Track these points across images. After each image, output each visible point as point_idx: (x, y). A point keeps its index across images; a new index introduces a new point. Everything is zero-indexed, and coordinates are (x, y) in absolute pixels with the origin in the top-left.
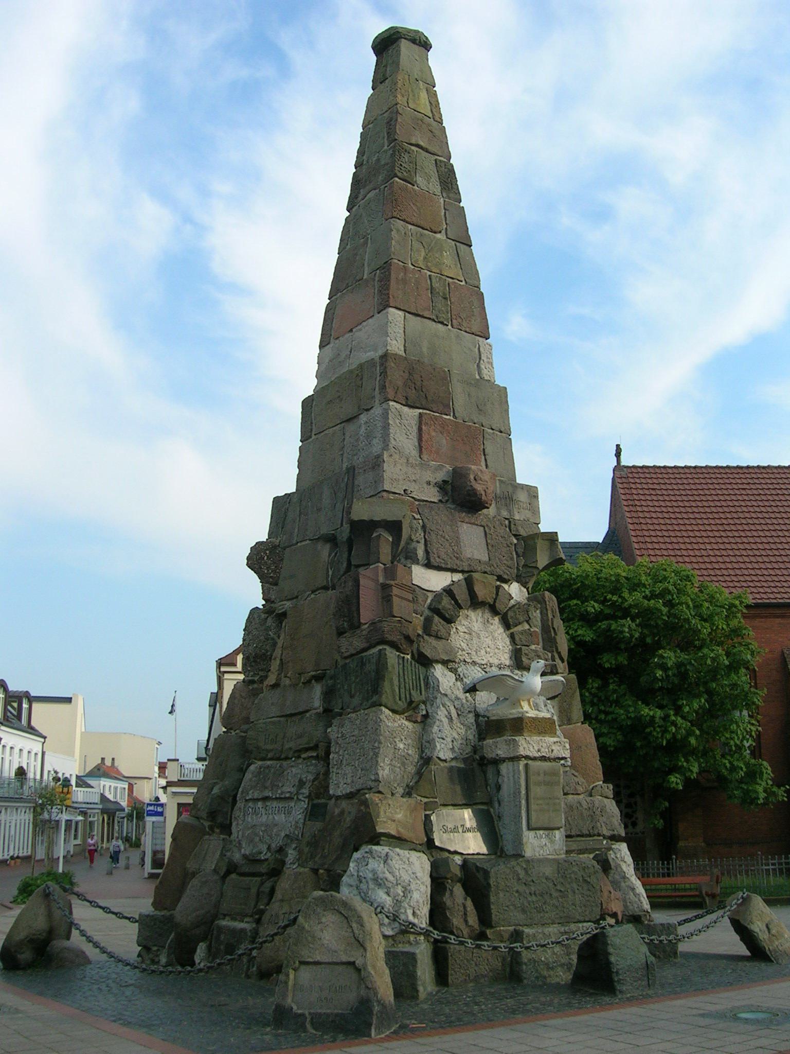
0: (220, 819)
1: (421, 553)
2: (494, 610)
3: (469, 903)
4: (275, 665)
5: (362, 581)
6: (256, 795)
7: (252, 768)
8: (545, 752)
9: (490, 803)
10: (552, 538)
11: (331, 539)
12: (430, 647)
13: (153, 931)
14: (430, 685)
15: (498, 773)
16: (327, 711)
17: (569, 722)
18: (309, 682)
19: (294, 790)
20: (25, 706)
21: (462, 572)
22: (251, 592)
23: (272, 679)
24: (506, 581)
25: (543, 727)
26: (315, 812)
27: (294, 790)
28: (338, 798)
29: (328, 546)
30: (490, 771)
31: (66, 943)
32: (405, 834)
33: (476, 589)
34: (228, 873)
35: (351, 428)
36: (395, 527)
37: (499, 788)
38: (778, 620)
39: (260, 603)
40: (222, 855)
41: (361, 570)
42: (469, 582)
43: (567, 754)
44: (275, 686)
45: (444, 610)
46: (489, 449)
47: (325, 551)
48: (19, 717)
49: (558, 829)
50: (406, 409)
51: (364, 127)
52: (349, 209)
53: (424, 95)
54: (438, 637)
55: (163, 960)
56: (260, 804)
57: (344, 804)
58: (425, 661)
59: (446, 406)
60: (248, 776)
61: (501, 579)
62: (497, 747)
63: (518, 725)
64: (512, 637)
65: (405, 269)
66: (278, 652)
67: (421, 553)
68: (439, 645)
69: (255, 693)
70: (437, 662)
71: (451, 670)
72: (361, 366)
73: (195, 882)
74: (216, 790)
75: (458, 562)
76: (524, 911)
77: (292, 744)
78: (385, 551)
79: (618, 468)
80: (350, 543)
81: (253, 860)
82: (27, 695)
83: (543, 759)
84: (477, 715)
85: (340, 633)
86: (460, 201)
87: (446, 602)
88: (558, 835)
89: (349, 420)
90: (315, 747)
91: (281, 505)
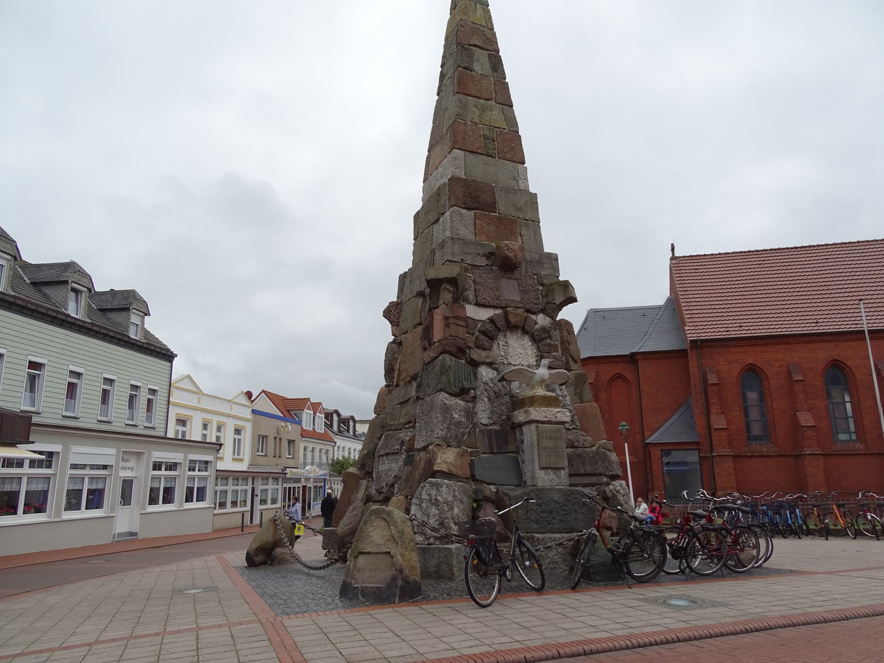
0: (367, 469)
1: (471, 297)
2: (525, 332)
6: (382, 452)
8: (550, 418)
9: (517, 452)
11: (421, 294)
12: (477, 354)
16: (418, 398)
18: (410, 382)
19: (398, 447)
20: (351, 424)
21: (502, 308)
22: (385, 333)
24: (534, 313)
26: (409, 461)
27: (398, 447)
28: (419, 450)
30: (518, 430)
32: (454, 471)
33: (510, 317)
35: (436, 227)
36: (453, 281)
37: (523, 442)
38: (783, 346)
42: (506, 314)
43: (568, 419)
44: (397, 386)
45: (491, 332)
46: (524, 232)
47: (420, 301)
48: (348, 431)
49: (563, 468)
50: (465, 211)
51: (446, 40)
53: (480, 11)
54: (485, 349)
56: (385, 458)
58: (475, 364)
59: (492, 207)
61: (528, 311)
62: (520, 416)
63: (532, 401)
67: (471, 297)
68: (483, 354)
69: (390, 392)
70: (483, 363)
71: (494, 369)
73: (351, 508)
75: (498, 302)
76: (537, 522)
79: (673, 258)
82: (352, 418)
83: (550, 422)
84: (512, 397)
85: (425, 349)
86: (505, 78)
87: (489, 326)
88: (563, 474)
90: (410, 422)
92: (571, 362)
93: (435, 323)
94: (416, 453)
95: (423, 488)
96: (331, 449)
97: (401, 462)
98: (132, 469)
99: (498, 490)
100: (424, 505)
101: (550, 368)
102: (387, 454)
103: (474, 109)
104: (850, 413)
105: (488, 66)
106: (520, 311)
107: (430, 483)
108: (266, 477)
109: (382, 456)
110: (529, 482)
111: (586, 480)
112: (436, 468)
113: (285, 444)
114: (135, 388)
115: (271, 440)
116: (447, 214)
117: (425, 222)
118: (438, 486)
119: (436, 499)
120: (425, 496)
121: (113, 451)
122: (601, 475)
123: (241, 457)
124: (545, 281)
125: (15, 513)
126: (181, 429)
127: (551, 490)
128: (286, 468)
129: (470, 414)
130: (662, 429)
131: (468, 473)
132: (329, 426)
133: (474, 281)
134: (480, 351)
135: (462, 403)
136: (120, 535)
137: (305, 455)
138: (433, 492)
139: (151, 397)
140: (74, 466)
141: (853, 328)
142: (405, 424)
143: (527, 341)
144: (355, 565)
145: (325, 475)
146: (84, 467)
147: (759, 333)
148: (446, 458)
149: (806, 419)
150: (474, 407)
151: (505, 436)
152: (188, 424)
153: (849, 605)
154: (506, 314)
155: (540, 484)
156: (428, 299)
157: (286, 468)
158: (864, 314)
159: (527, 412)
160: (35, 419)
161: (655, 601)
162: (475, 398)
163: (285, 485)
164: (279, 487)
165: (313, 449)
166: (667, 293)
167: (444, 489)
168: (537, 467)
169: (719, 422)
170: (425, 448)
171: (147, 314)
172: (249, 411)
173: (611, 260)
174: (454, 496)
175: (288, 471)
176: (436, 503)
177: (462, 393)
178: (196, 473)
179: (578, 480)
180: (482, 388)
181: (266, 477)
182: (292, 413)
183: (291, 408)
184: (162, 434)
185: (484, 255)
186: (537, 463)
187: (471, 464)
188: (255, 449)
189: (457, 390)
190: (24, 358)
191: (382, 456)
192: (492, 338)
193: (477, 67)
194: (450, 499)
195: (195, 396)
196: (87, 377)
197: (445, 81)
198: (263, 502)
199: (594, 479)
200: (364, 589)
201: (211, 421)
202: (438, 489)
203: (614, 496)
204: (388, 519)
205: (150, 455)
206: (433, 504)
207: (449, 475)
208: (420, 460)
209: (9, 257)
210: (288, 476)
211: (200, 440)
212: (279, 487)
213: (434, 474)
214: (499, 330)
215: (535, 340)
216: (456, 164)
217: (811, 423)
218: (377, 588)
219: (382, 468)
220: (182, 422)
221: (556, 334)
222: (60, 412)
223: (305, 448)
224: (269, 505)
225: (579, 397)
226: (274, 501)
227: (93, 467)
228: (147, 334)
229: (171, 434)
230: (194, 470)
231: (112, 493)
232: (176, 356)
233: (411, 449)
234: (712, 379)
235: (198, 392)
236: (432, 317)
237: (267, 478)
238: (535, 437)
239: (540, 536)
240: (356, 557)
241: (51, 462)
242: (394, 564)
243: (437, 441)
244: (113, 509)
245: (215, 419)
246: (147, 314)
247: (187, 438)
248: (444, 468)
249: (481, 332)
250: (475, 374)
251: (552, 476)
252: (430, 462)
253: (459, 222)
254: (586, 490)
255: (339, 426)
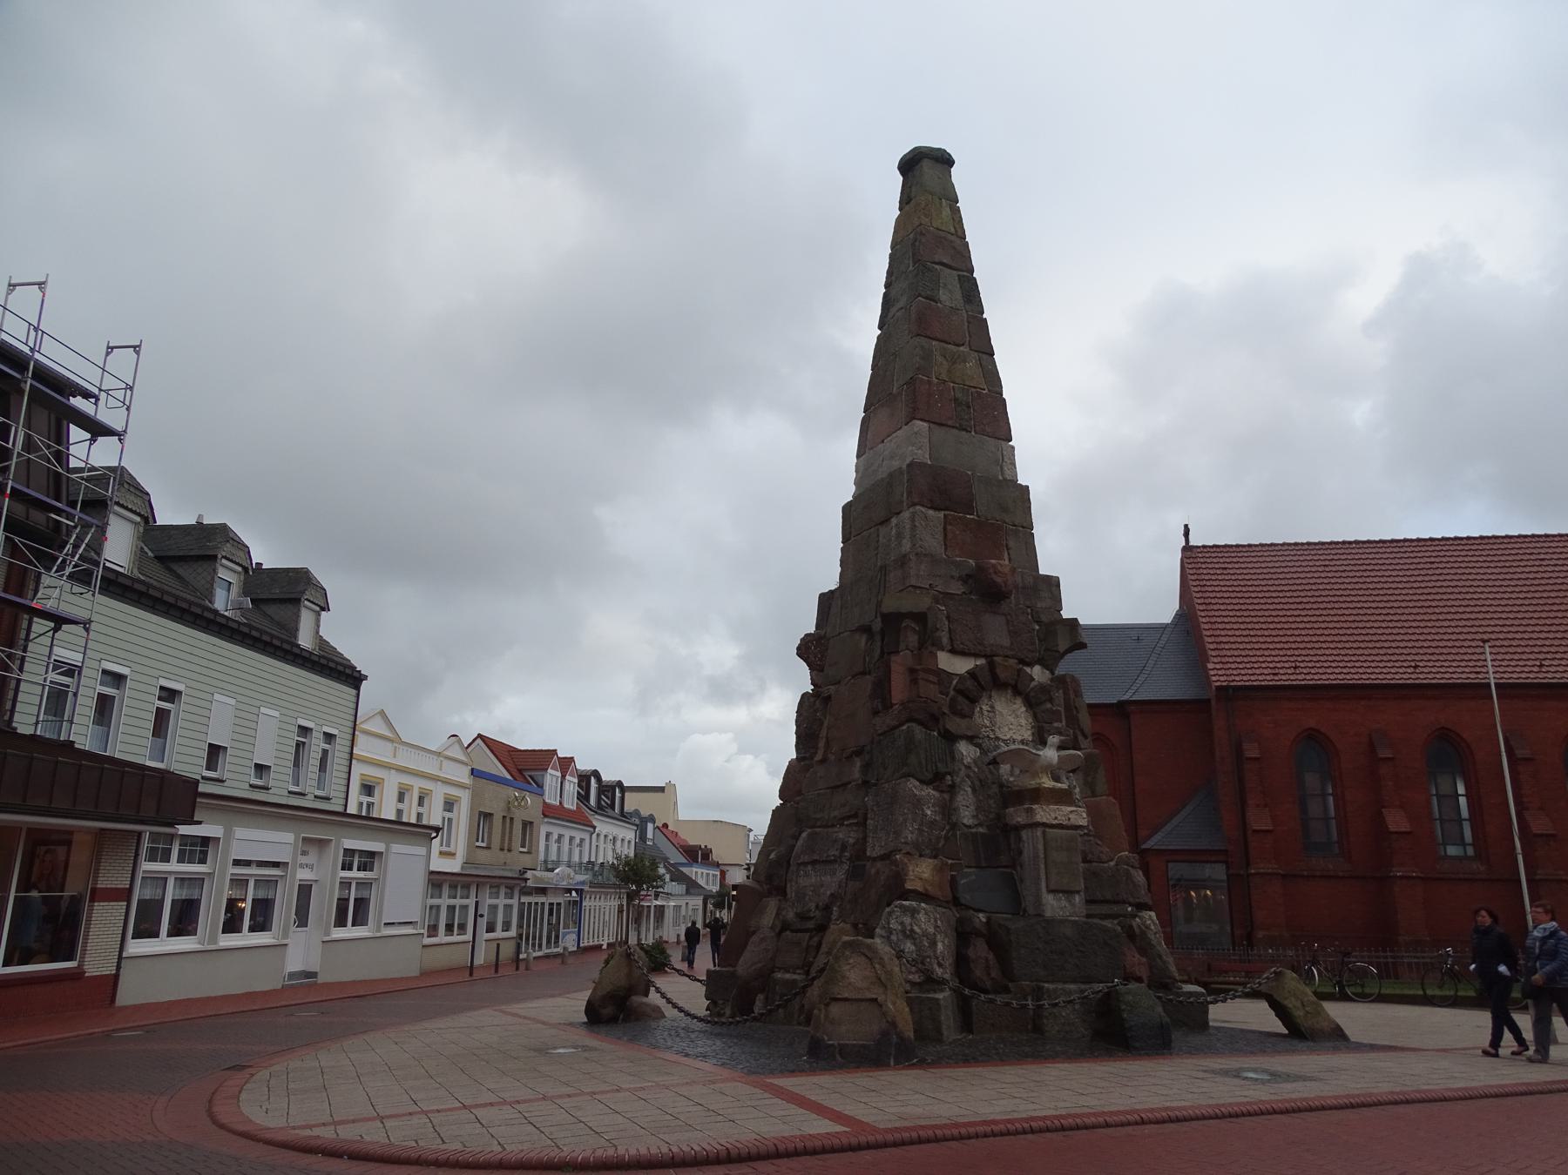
1: (945, 640)
2: (1017, 692)
3: (991, 956)
4: (822, 744)
5: (894, 667)
6: (806, 858)
7: (804, 835)
10: (1074, 622)
11: (866, 630)
12: (954, 724)
13: (715, 985)
14: (953, 755)
15: (1020, 839)
16: (866, 783)
17: (1094, 795)
18: (849, 758)
20: (618, 794)
21: (985, 656)
23: (819, 757)
25: (1063, 797)
26: (856, 873)
28: (874, 859)
29: (864, 638)
31: (645, 1000)
34: (783, 929)
35: (883, 530)
36: (920, 618)
37: (1020, 853)
39: (809, 688)
40: (778, 914)
41: (893, 658)
42: (992, 666)
43: (1084, 823)
44: (823, 761)
46: (1011, 544)
48: (612, 806)
50: (931, 512)
51: (892, 248)
52: (880, 328)
53: (946, 212)
54: (963, 716)
55: (728, 1012)
57: (879, 864)
58: (951, 738)
60: (800, 842)
61: (1022, 662)
62: (1017, 816)
63: (1037, 795)
64: (1035, 716)
65: (929, 383)
66: (824, 733)
67: (945, 640)
68: (963, 723)
72: (891, 475)
73: (754, 938)
74: (772, 856)
77: (836, 813)
78: (913, 639)
79: (1187, 549)
80: (883, 632)
81: (803, 917)
82: (620, 784)
84: (1001, 786)
85: (876, 713)
87: (969, 684)
89: (882, 523)
90: (855, 816)
91: (826, 600)
92: (1080, 738)
93: (894, 676)
94: (868, 864)
95: (890, 914)
96: (586, 836)
97: (841, 874)
98: (311, 867)
99: (989, 919)
100: (894, 938)
101: (1060, 748)
102: (814, 862)
103: (940, 359)
104: (1465, 813)
105: (958, 294)
106: (1012, 662)
107: (901, 906)
108: (495, 883)
109: (805, 864)
110: (1031, 911)
111: (1104, 909)
112: (908, 886)
113: (518, 827)
114: (304, 731)
115: (497, 821)
116: (906, 514)
117: (860, 522)
118: (913, 912)
119: (912, 930)
120: (894, 925)
121: (289, 837)
122: (1124, 902)
123: (451, 849)
124: (1044, 618)
125: (157, 936)
126: (366, 799)
127: (1063, 922)
128: (525, 870)
129: (947, 810)
130: (1168, 827)
131: (950, 897)
132: (583, 797)
133: (948, 618)
134: (958, 720)
135: (937, 794)
136: (292, 975)
137: (547, 847)
138: (907, 920)
139: (327, 746)
140: (237, 863)
141: (1473, 679)
142: (844, 819)
143: (1019, 707)
144: (826, 1016)
145: (583, 883)
146: (248, 863)
147: (1324, 680)
148: (921, 872)
149: (1396, 821)
150: (952, 799)
151: (999, 844)
152: (377, 792)
153: (1474, 1084)
154: (992, 666)
155: (1048, 914)
156: (878, 638)
157: (525, 870)
158: (1489, 658)
159: (1030, 811)
160: (202, 788)
161: (1226, 1073)
162: (953, 786)
163: (525, 899)
164: (514, 902)
165: (560, 836)
166: (1174, 606)
167: (922, 916)
168: (1044, 889)
169: (1259, 820)
170: (885, 857)
171: (325, 608)
172: (467, 770)
173: (1108, 567)
174: (936, 927)
175: (529, 874)
176: (910, 935)
177: (935, 780)
178: (174, 866)
179: (1096, 909)
180: (962, 773)
181: (495, 883)
182: (526, 774)
183: (526, 766)
184: (340, 809)
185: (960, 578)
186: (1043, 884)
187: (953, 882)
188: (475, 834)
189: (930, 776)
190: (153, 681)
191: (805, 864)
192: (973, 701)
193: (943, 295)
194: (931, 930)
195: (389, 745)
196: (189, 700)
197: (893, 310)
198: (491, 929)
199: (1115, 909)
200: (842, 1048)
201: (409, 788)
202: (913, 916)
203: (1143, 933)
204: (871, 956)
205: (338, 843)
206: (907, 937)
207: (924, 897)
208: (878, 872)
209: (138, 519)
210: (529, 883)
211: (393, 818)
212: (514, 902)
213: (906, 894)
214: (983, 689)
215: (1030, 704)
216: (914, 443)
217: (1405, 827)
218: (863, 1046)
219: (803, 882)
220: (368, 789)
221: (1059, 695)
222: (246, 778)
223: (548, 835)
224: (499, 934)
225: (1090, 788)
226: (507, 927)
227: (261, 864)
228: (323, 643)
229: (352, 809)
230: (350, 869)
231: (283, 910)
232: (366, 678)
233: (859, 854)
234: (1251, 751)
235: (395, 739)
236: (889, 667)
237: (498, 887)
238: (1041, 847)
239: (1051, 986)
240: (827, 1005)
241: (205, 853)
242: (884, 1014)
243: (908, 849)
244: (286, 935)
245: (417, 784)
246: (325, 608)
247: (375, 815)
248: (919, 886)
249: (959, 691)
250: (952, 753)
251: (1064, 903)
252: (899, 877)
253: (925, 529)
254: (1107, 923)
255: (599, 799)
